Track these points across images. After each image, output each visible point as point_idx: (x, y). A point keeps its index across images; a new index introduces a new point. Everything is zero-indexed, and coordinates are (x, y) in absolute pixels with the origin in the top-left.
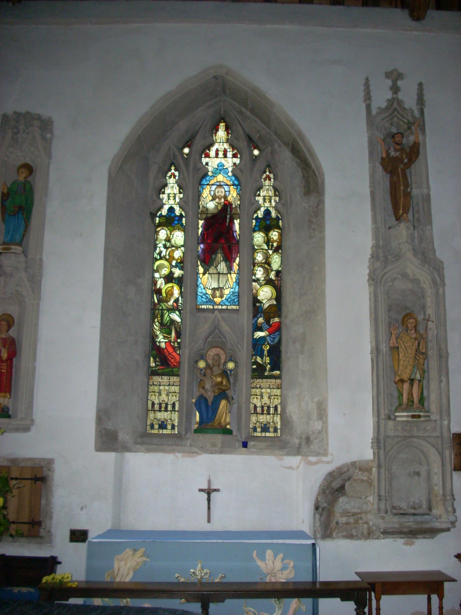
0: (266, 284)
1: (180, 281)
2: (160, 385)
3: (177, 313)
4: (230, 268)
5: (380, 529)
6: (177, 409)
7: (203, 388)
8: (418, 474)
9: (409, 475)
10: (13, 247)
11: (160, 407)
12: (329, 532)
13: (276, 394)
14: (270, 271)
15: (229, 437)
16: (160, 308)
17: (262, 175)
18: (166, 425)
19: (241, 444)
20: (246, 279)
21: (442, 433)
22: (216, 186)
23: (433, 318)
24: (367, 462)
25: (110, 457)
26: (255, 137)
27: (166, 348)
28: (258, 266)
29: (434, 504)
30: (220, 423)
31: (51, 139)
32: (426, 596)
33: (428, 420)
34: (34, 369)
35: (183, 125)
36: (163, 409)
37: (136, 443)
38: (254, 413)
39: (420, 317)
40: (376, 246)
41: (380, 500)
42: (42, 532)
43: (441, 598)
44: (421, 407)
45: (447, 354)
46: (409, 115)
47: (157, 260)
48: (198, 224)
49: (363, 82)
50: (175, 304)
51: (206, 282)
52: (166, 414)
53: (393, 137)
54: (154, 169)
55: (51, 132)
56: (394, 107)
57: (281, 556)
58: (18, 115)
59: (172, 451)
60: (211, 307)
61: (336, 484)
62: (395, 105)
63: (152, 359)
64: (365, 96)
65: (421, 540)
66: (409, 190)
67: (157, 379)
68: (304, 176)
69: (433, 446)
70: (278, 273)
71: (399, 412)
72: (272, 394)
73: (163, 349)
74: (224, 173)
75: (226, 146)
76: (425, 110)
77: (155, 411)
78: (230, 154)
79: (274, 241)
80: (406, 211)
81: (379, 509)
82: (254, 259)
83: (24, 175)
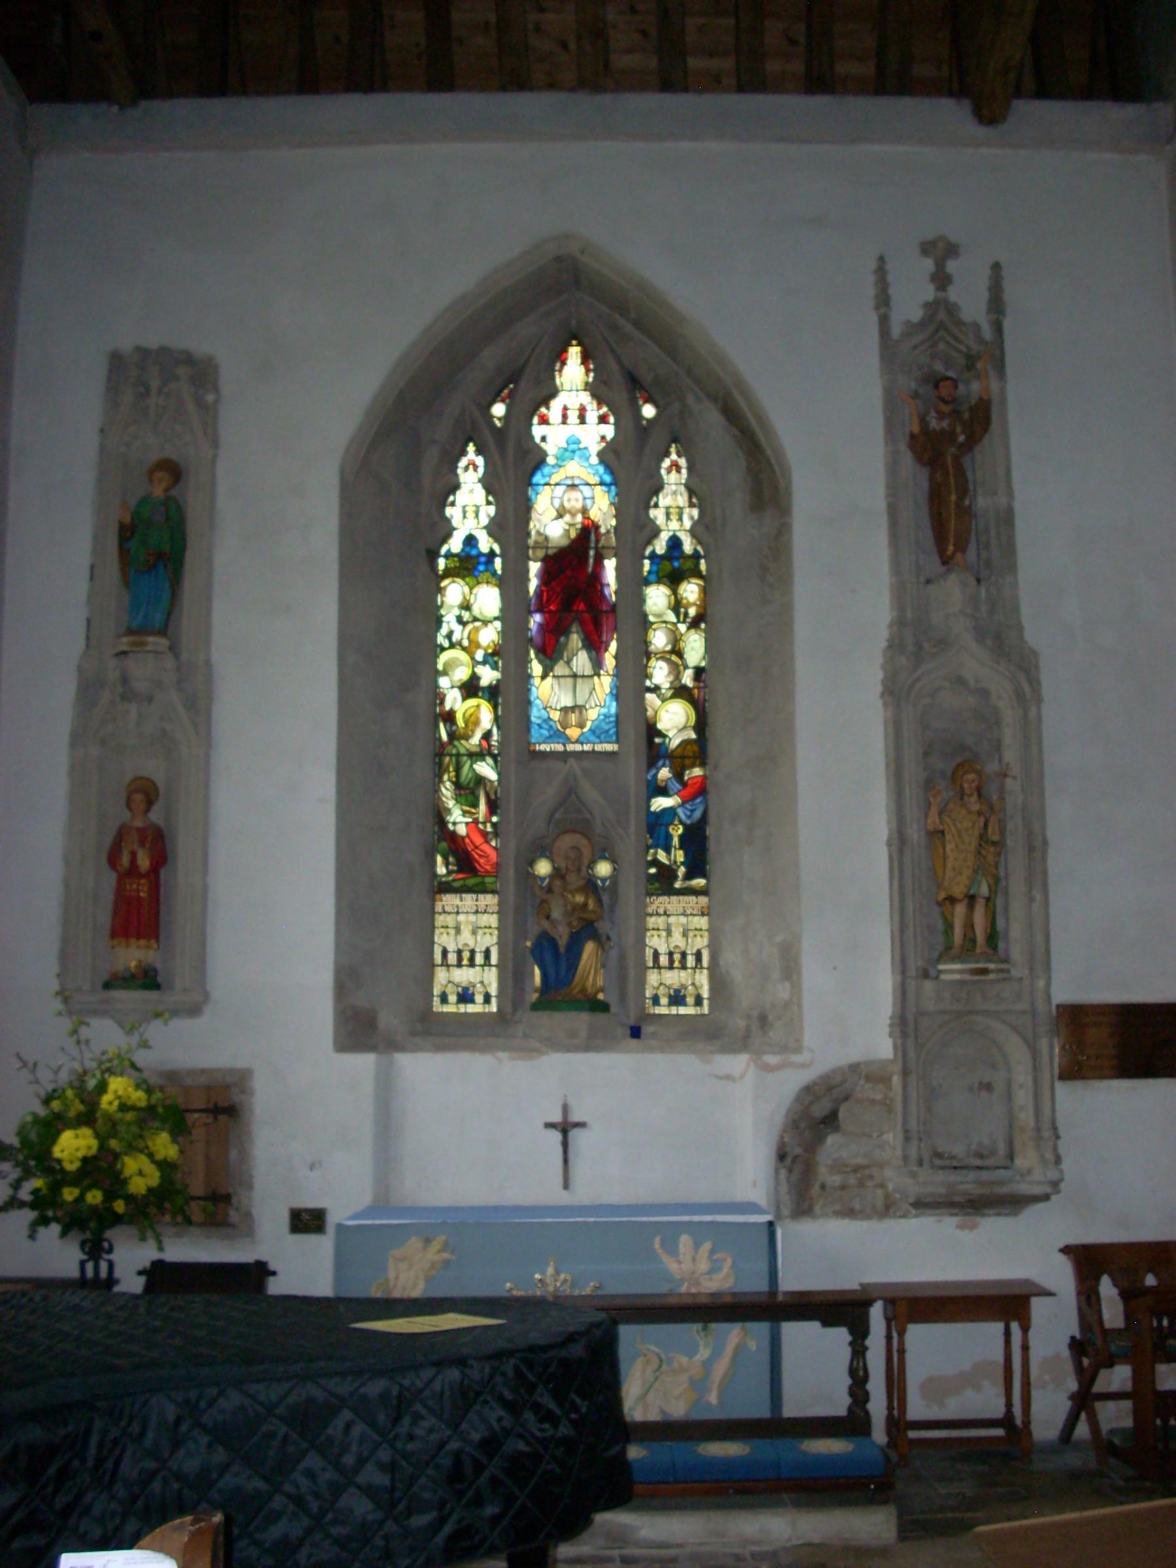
0: (673, 697)
1: (492, 693)
2: (458, 913)
3: (489, 760)
4: (598, 664)
5: (907, 1196)
6: (494, 959)
7: (548, 917)
8: (988, 1087)
9: (971, 1089)
10: (151, 639)
11: (460, 959)
12: (806, 1205)
13: (698, 927)
14: (682, 668)
15: (601, 1017)
16: (454, 751)
17: (662, 460)
18: (473, 994)
19: (629, 1032)
20: (632, 686)
21: (1033, 1004)
22: (563, 488)
23: (1015, 769)
24: (884, 1063)
25: (365, 1062)
26: (647, 378)
27: (468, 835)
28: (657, 659)
29: (1018, 1146)
30: (583, 990)
31: (217, 402)
32: (999, 1327)
33: (1005, 980)
34: (205, 889)
35: (491, 357)
36: (465, 962)
37: (413, 1033)
38: (654, 967)
39: (992, 767)
40: (899, 623)
41: (907, 1139)
42: (234, 1217)
43: (1025, 1329)
44: (990, 951)
45: (1045, 843)
46: (971, 336)
47: (443, 649)
48: (527, 571)
49: (873, 265)
50: (485, 744)
51: (548, 693)
52: (471, 971)
53: (936, 386)
54: (431, 456)
55: (216, 390)
56: (940, 318)
57: (707, 1246)
58: (143, 353)
59: (485, 1049)
60: (560, 748)
61: (820, 1110)
62: (942, 315)
63: (439, 859)
64: (876, 297)
65: (992, 1219)
66: (967, 502)
67: (449, 901)
68: (749, 469)
69: (1015, 1029)
70: (699, 672)
71: (945, 963)
72: (691, 927)
73: (463, 838)
74: (580, 457)
75: (585, 398)
76: (1007, 324)
77: (448, 966)
78: (592, 415)
79: (689, 605)
80: (961, 547)
81: (905, 1158)
82: (647, 643)
83: (164, 485)
